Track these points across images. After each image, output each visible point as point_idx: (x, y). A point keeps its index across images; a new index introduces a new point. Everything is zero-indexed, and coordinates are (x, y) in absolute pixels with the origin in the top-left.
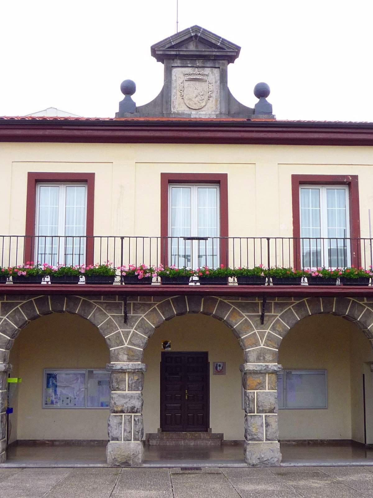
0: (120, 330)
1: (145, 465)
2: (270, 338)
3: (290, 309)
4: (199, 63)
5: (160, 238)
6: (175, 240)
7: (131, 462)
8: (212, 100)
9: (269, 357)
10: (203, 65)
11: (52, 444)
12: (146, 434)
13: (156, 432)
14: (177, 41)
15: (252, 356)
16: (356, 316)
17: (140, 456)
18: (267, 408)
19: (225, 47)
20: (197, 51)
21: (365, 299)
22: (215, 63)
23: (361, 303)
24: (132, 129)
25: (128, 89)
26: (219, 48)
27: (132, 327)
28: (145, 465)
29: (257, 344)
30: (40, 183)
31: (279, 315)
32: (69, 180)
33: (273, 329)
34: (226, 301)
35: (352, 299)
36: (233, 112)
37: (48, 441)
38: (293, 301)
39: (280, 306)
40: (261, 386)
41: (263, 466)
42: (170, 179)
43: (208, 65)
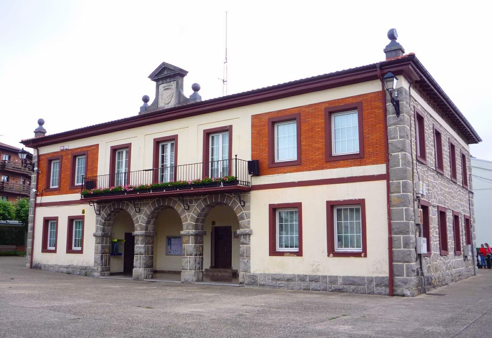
0: (187, 214)
1: (145, 280)
2: (192, 217)
3: (200, 202)
4: (168, 80)
5: (170, 168)
6: (133, 173)
7: (139, 278)
8: (174, 97)
9: (190, 227)
10: (170, 81)
11: (169, 272)
12: (205, 269)
13: (209, 268)
14: (158, 72)
15: (184, 227)
16: (228, 204)
17: (143, 275)
18: (189, 253)
19: (175, 70)
20: (167, 75)
21: (233, 194)
22: (174, 79)
23: (231, 196)
24: (149, 117)
25: (146, 99)
26: (173, 70)
27: (142, 214)
28: (145, 280)
29: (186, 220)
30: (278, 123)
31: (196, 205)
32: (285, 120)
33: (193, 213)
34: (175, 199)
35: (227, 194)
36: (181, 102)
37: (168, 271)
38: (202, 197)
39: (196, 200)
40: (188, 242)
41: (186, 283)
42: (331, 110)
43: (171, 80)
